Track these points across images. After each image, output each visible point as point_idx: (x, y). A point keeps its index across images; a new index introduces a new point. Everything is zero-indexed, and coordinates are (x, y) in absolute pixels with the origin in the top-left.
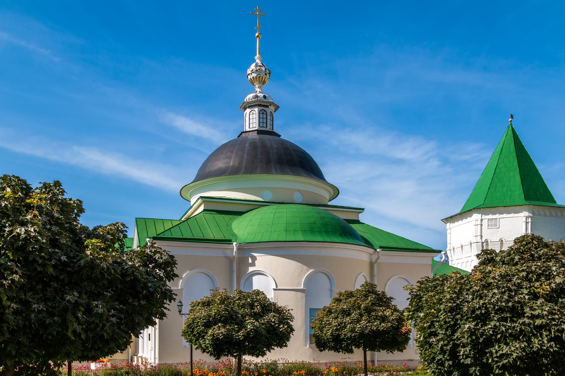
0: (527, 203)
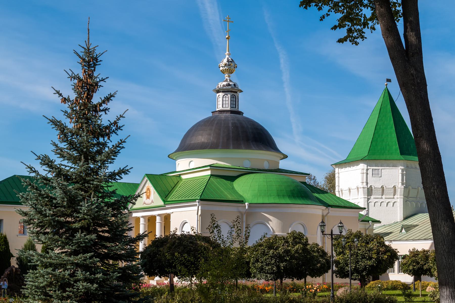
0: (402, 157)
